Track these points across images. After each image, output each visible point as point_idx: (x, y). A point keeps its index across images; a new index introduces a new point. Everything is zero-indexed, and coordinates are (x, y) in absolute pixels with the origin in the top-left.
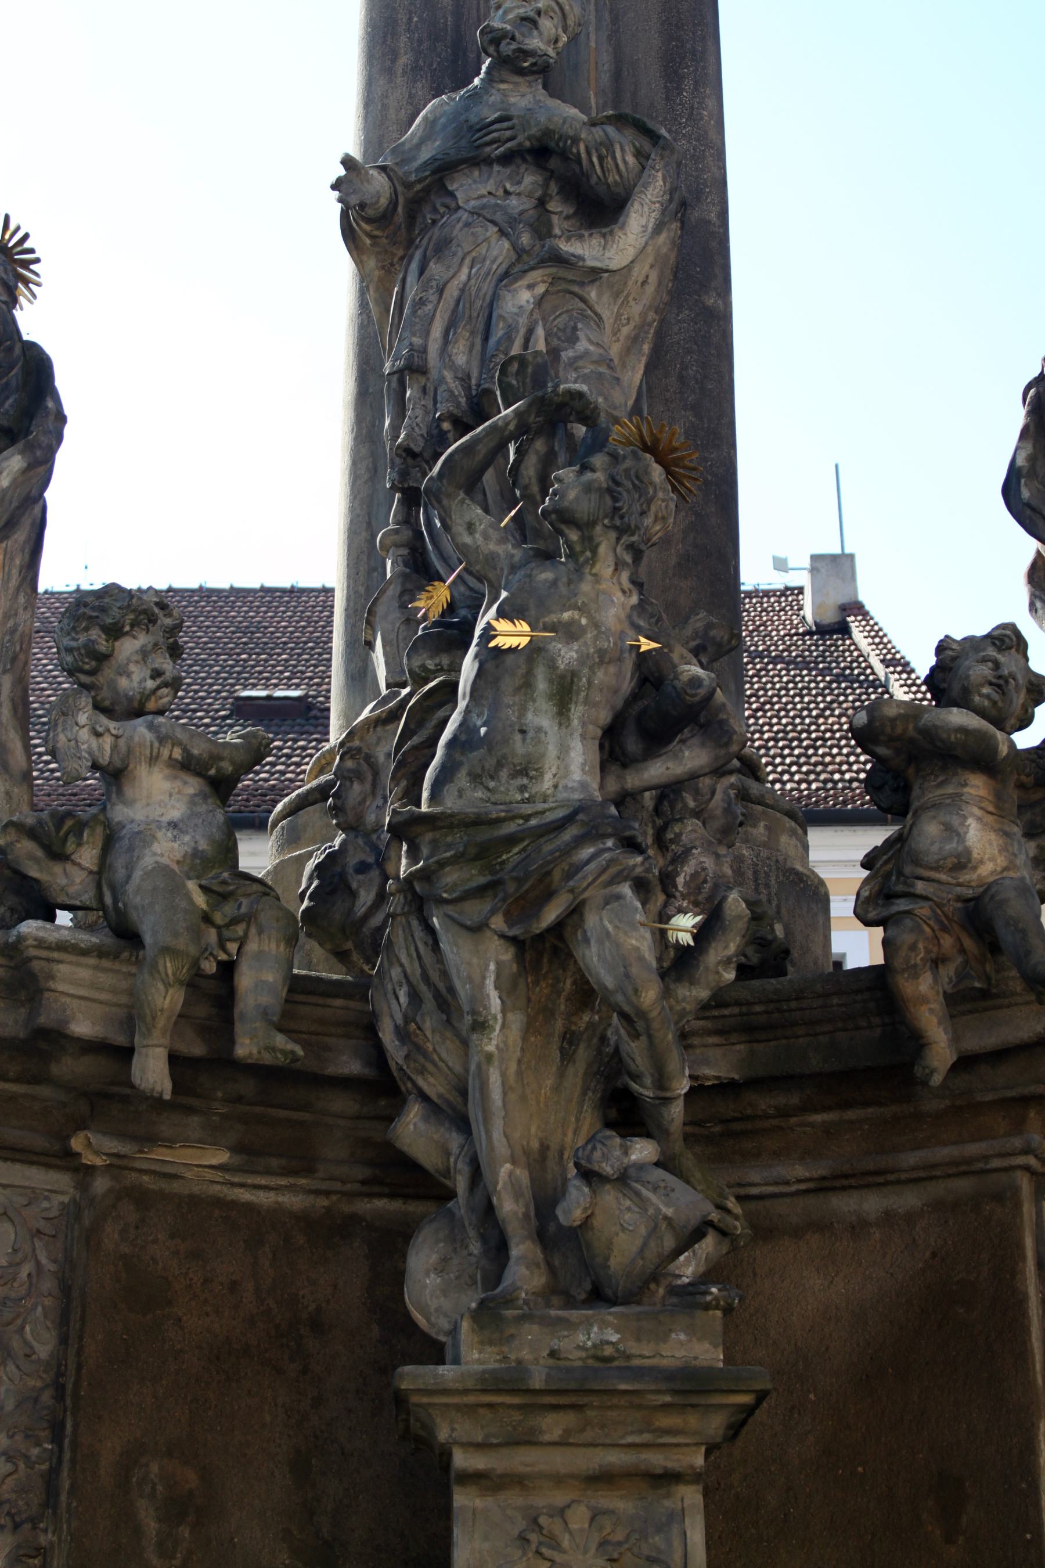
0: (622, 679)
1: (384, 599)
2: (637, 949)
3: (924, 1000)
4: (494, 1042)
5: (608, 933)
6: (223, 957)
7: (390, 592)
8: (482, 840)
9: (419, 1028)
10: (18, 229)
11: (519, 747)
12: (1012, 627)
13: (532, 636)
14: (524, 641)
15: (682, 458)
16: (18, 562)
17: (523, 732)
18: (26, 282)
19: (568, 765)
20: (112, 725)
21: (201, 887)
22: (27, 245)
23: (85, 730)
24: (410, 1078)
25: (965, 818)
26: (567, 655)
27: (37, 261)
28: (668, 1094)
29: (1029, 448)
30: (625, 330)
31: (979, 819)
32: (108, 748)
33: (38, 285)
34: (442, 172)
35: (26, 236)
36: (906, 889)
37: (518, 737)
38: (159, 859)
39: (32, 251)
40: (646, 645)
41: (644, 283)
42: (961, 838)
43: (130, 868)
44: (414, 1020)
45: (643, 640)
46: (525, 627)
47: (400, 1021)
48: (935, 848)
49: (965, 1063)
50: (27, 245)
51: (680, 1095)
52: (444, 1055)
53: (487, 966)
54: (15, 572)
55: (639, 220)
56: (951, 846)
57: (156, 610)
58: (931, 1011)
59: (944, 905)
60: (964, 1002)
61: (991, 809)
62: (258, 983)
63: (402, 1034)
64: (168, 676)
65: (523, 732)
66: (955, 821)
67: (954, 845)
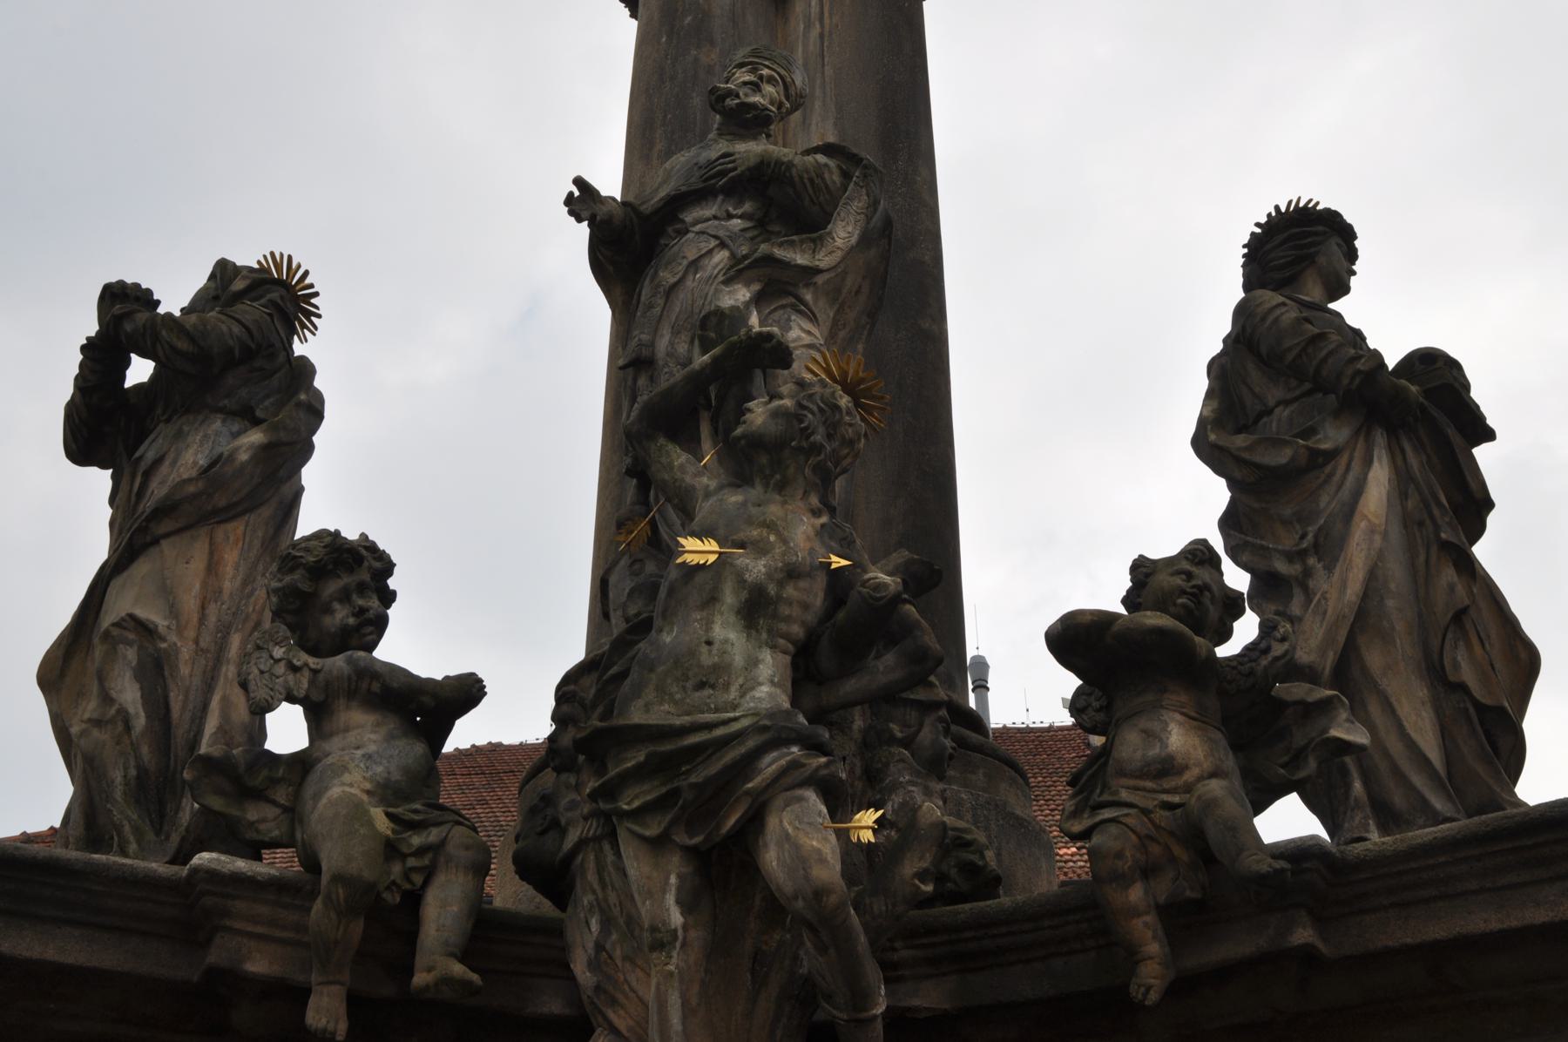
0: (815, 594)
1: (617, 568)
2: (819, 851)
3: (1135, 913)
4: (674, 960)
5: (787, 835)
6: (408, 886)
7: (622, 563)
8: (671, 754)
9: (611, 957)
10: (299, 266)
11: (707, 658)
12: (1204, 542)
13: (720, 554)
14: (712, 558)
15: (869, 389)
16: (260, 534)
17: (709, 643)
18: (308, 314)
19: (763, 684)
20: (312, 661)
21: (387, 814)
22: (308, 281)
23: (282, 664)
24: (601, 1012)
25: (1167, 724)
26: (757, 568)
27: (316, 294)
28: (864, 1015)
29: (1215, 404)
30: (842, 334)
31: (1180, 724)
32: (305, 685)
33: (319, 316)
34: (677, 203)
35: (306, 273)
36: (1110, 798)
37: (704, 649)
38: (347, 789)
39: (311, 286)
40: (838, 562)
41: (858, 292)
42: (1165, 745)
43: (317, 796)
44: (604, 949)
45: (834, 558)
46: (714, 546)
47: (591, 951)
48: (1139, 754)
49: (1181, 987)
50: (308, 281)
51: (875, 1017)
52: (634, 984)
53: (668, 878)
54: (257, 543)
55: (844, 232)
56: (1155, 751)
57: (364, 552)
58: (1146, 924)
59: (1151, 812)
60: (1180, 919)
61: (1193, 714)
62: (442, 912)
63: (594, 965)
64: (371, 614)
65: (709, 643)
66: (1155, 726)
67: (1157, 750)
